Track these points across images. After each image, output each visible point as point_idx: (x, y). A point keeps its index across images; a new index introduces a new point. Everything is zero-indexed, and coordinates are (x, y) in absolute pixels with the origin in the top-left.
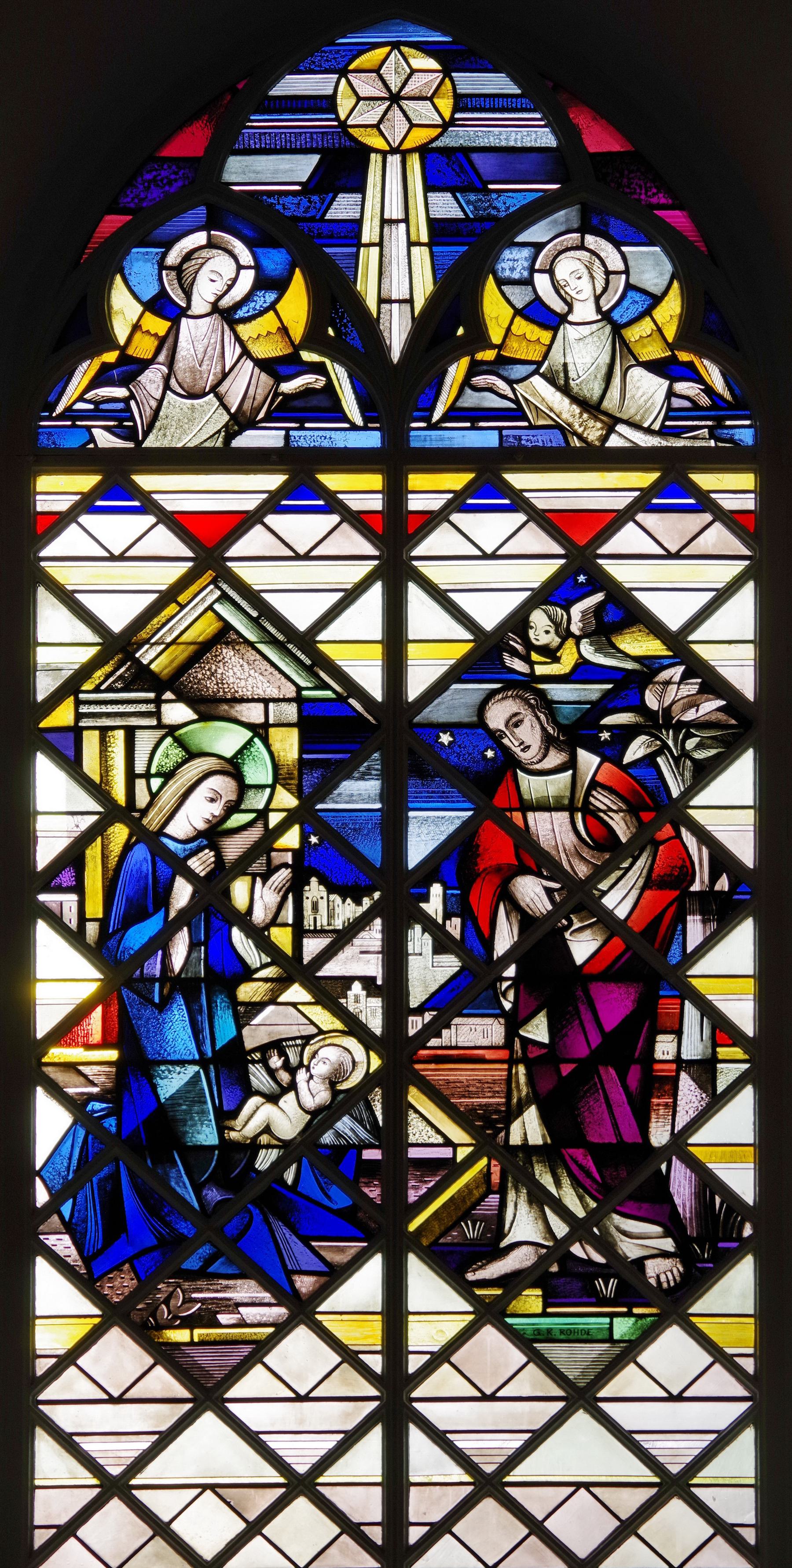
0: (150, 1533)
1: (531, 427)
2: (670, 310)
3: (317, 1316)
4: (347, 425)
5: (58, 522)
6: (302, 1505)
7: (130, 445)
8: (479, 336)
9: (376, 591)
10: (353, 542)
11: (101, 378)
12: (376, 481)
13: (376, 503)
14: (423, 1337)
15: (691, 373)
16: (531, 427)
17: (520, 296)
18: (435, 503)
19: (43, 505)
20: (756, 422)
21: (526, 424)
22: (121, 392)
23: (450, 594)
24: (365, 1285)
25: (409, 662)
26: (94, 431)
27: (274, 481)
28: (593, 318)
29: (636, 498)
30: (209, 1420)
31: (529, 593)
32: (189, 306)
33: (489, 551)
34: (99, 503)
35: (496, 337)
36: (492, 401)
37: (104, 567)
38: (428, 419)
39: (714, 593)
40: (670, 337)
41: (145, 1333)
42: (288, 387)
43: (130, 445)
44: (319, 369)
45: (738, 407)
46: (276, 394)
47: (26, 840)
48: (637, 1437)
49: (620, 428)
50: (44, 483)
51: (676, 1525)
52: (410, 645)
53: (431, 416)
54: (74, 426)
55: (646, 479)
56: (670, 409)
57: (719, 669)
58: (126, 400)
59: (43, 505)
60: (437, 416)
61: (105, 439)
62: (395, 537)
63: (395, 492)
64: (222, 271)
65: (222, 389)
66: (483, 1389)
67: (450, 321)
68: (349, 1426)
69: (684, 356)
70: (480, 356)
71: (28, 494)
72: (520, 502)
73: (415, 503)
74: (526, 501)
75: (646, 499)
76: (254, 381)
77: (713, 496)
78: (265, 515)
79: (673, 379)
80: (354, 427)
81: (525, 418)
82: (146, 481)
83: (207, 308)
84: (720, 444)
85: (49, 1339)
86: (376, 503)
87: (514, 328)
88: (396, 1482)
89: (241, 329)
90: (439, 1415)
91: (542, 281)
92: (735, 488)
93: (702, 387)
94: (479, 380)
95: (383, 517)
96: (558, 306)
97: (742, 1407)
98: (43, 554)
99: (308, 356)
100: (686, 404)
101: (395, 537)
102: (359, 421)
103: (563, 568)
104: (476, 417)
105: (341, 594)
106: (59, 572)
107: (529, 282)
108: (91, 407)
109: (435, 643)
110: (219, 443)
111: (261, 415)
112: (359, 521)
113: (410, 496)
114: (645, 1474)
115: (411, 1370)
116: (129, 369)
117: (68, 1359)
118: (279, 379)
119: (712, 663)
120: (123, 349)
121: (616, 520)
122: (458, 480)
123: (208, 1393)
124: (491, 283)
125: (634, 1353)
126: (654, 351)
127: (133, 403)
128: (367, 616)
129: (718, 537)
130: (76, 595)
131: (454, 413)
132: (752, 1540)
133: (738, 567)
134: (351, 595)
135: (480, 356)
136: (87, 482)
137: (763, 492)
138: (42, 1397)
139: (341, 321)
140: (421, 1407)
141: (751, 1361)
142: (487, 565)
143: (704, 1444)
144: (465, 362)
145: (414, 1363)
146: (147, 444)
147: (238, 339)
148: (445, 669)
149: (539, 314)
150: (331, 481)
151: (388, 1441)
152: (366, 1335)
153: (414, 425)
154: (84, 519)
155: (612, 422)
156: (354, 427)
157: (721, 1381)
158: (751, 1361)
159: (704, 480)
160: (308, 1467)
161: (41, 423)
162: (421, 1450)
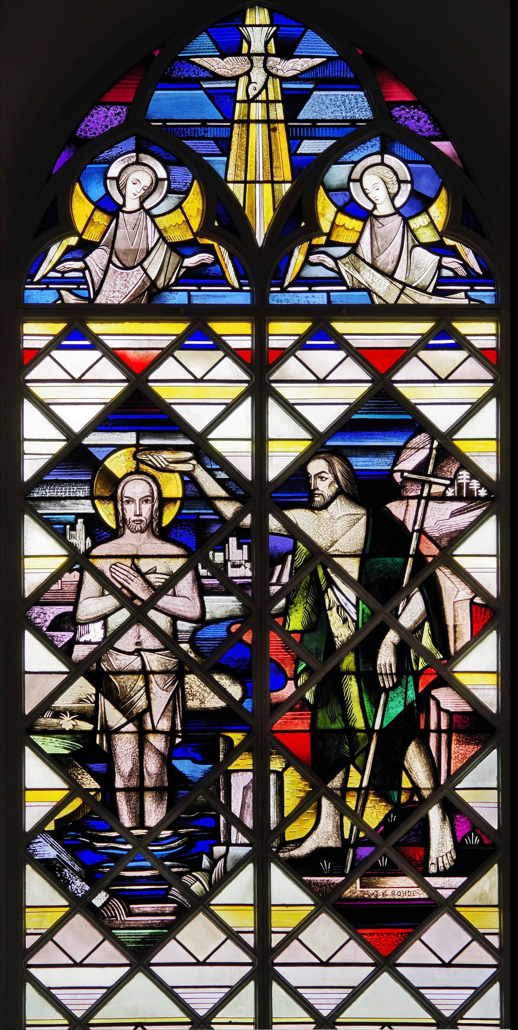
1: (349, 290)
3: (211, 907)
5: (38, 355)
9: (247, 404)
10: (229, 369)
12: (246, 327)
13: (246, 343)
14: (281, 921)
15: (454, 253)
18: (286, 343)
19: (28, 343)
22: (79, 265)
23: (296, 407)
24: (241, 887)
26: (62, 292)
28: (390, 229)
29: (50, 341)
32: (124, 205)
34: (65, 343)
35: (326, 227)
37: (69, 390)
38: (281, 285)
39: (470, 406)
41: (96, 917)
42: (190, 262)
44: (210, 249)
45: (485, 278)
47: (16, 456)
48: (422, 991)
49: (408, 290)
50: (28, 328)
53: (284, 283)
54: (48, 288)
55: (425, 327)
56: (440, 277)
58: (82, 270)
60: (286, 284)
61: (70, 299)
62: (260, 367)
63: (260, 335)
65: (145, 264)
67: (296, 218)
68: (233, 982)
69: (449, 242)
70: (315, 241)
71: (18, 336)
74: (346, 342)
75: (425, 341)
76: (167, 259)
77: (468, 338)
79: (441, 256)
80: (234, 290)
81: (344, 283)
82: (95, 327)
84: (472, 302)
85: (36, 923)
86: (246, 343)
87: (337, 222)
90: (292, 976)
93: (462, 263)
96: (368, 206)
97: (247, 969)
100: (451, 274)
101: (260, 367)
102: (237, 285)
104: (312, 283)
106: (39, 391)
107: (348, 189)
108: (60, 275)
111: (173, 280)
112: (236, 355)
113: (270, 338)
115: (273, 945)
116: (86, 248)
117: (47, 937)
118: (183, 257)
122: (302, 327)
123: (140, 957)
124: (321, 190)
126: (428, 236)
127: (87, 272)
128: (241, 420)
129: (474, 368)
131: (299, 280)
134: (231, 407)
135: (315, 241)
137: (500, 336)
139: (224, 217)
144: (305, 246)
145: (276, 939)
146: (98, 301)
147: (156, 226)
148: (292, 459)
149: (351, 209)
150: (218, 327)
152: (244, 921)
153: (272, 289)
154: (54, 353)
157: (477, 954)
159: (463, 328)
160: (206, 1011)
161: (26, 286)
162: (276, 415)
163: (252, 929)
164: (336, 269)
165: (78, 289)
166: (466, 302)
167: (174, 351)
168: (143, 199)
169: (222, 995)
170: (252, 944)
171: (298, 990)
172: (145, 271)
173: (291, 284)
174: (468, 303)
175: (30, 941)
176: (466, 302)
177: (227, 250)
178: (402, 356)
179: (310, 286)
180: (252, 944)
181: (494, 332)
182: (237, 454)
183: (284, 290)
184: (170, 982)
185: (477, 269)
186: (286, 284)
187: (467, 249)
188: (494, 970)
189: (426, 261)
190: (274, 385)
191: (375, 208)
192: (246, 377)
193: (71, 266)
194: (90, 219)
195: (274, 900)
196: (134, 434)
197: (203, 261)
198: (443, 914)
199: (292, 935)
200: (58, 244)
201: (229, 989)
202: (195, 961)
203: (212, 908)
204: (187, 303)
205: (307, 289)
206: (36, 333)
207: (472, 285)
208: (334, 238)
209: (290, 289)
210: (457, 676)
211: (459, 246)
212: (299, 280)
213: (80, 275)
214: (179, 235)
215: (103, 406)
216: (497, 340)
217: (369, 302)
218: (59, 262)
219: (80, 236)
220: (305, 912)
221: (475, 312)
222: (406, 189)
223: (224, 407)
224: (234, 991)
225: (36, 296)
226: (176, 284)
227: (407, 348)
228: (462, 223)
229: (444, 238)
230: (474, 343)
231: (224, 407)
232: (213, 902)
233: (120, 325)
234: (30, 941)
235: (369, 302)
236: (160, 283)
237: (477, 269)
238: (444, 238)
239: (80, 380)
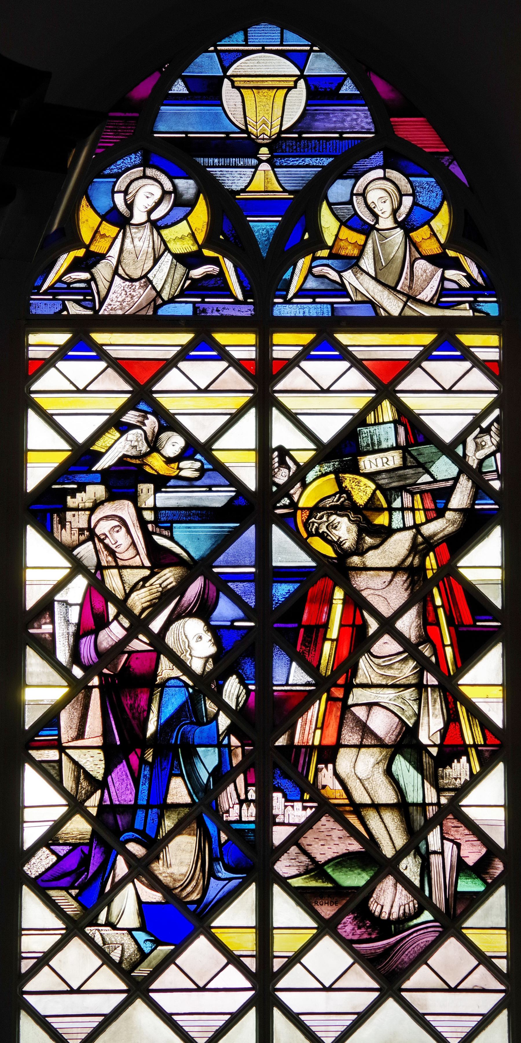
1: (352, 302)
4: (232, 300)
5: (45, 365)
7: (89, 312)
8: (318, 241)
10: (234, 379)
11: (75, 266)
12: (251, 338)
13: (250, 354)
14: (284, 945)
15: (457, 265)
16: (352, 302)
18: (290, 353)
19: (33, 353)
20: (499, 299)
21: (348, 300)
22: (85, 276)
23: (55, 417)
25: (28, 465)
27: (185, 338)
29: (421, 351)
30: (139, 1007)
31: (107, 417)
33: (325, 387)
37: (72, 402)
42: (197, 273)
43: (89, 312)
44: (215, 261)
46: (187, 278)
50: (33, 338)
55: (428, 338)
58: (87, 282)
59: (33, 353)
60: (290, 296)
61: (74, 309)
62: (264, 377)
63: (264, 346)
64: (146, 193)
68: (485, 1010)
69: (451, 253)
71: (24, 346)
72: (346, 353)
73: (278, 353)
74: (350, 353)
77: (472, 350)
81: (348, 296)
83: (144, 218)
84: (476, 314)
86: (250, 354)
87: (340, 236)
89: (164, 232)
92: (487, 345)
93: (465, 274)
96: (368, 218)
97: (249, 995)
99: (207, 253)
100: (455, 286)
101: (264, 377)
102: (240, 297)
105: (229, 417)
107: (351, 202)
108: (65, 286)
110: (150, 313)
112: (239, 365)
115: (276, 969)
116: (90, 261)
121: (166, 365)
124: (325, 204)
126: (431, 248)
127: (92, 283)
128: (245, 432)
129: (478, 380)
134: (235, 418)
136: (62, 338)
137: (505, 348)
141: (505, 961)
142: (324, 396)
144: (309, 258)
145: (277, 964)
148: (50, 470)
149: (353, 223)
150: (222, 338)
152: (245, 944)
153: (276, 300)
154: (304, 364)
156: (237, 302)
157: (482, 977)
158: (505, 961)
159: (466, 339)
161: (32, 297)
163: (505, 954)
165: (85, 300)
166: (470, 313)
167: (421, 362)
168: (150, 212)
169: (474, 1024)
170: (253, 969)
171: (425, 1017)
174: (472, 315)
175: (25, 966)
176: (470, 313)
178: (406, 367)
179: (314, 297)
180: (253, 969)
181: (497, 344)
183: (288, 302)
184: (168, 1009)
185: (480, 280)
186: (290, 296)
188: (502, 995)
190: (276, 395)
191: (377, 222)
192: (251, 387)
193: (78, 277)
195: (276, 923)
198: (197, 937)
199: (294, 959)
201: (481, 1017)
203: (213, 930)
207: (475, 297)
209: (295, 300)
210: (462, 689)
211: (461, 258)
214: (188, 247)
215: (351, 417)
219: (87, 247)
220: (308, 935)
221: (479, 324)
222: (408, 201)
223: (229, 417)
225: (42, 306)
227: (409, 360)
228: (465, 235)
229: (447, 250)
232: (465, 925)
234: (25, 966)
235: (373, 314)
236: (165, 295)
237: (480, 280)
238: (447, 250)
239: (206, 390)
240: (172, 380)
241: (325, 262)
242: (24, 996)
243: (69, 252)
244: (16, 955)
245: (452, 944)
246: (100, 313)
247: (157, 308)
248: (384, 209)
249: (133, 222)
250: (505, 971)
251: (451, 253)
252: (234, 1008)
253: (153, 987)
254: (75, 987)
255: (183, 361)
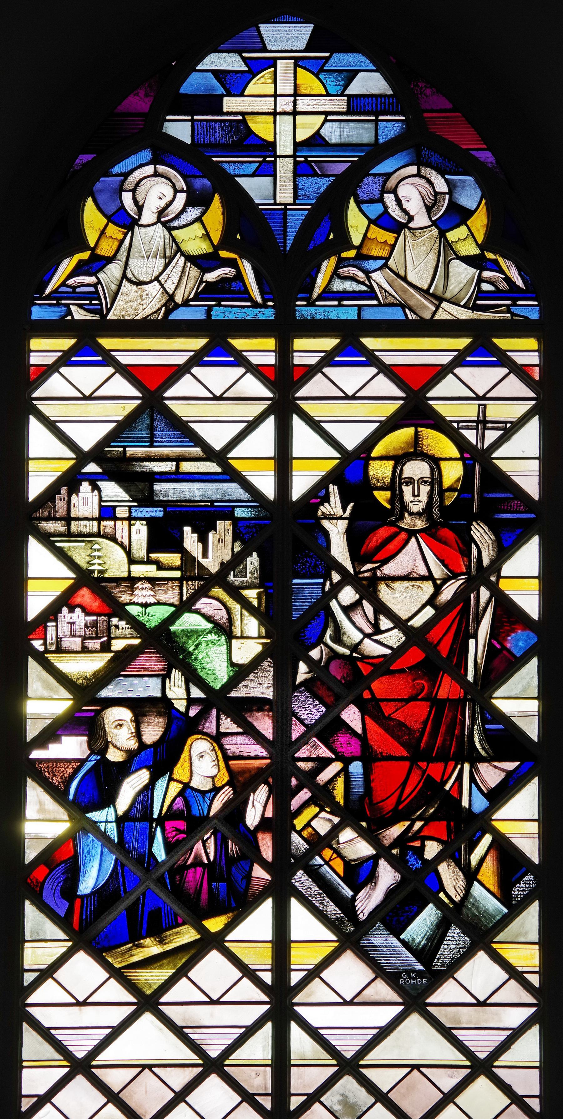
0: (105, 1100)
1: (380, 305)
2: (479, 222)
4: (249, 304)
5: (46, 372)
6: (214, 1080)
8: (344, 240)
9: (270, 423)
10: (253, 386)
11: (79, 270)
12: (270, 343)
13: (270, 359)
14: (302, 959)
17: (375, 210)
18: (312, 360)
19: (35, 359)
21: (375, 302)
22: (92, 280)
27: (198, 343)
28: (423, 242)
30: (148, 1019)
31: (115, 424)
35: (356, 240)
36: (349, 286)
40: (480, 239)
42: (211, 277)
46: (202, 281)
49: (444, 305)
50: (35, 343)
51: (483, 1094)
52: (294, 461)
57: (513, 478)
58: (95, 285)
59: (35, 359)
60: (315, 295)
61: (79, 314)
62: (285, 383)
63: (284, 352)
64: (156, 190)
66: (344, 1003)
69: (490, 256)
70: (344, 255)
73: (298, 359)
74: (377, 358)
77: (245, 354)
78: (192, 367)
79: (482, 269)
80: (255, 305)
81: (376, 298)
83: (154, 218)
86: (270, 359)
88: (281, 1063)
89: (174, 233)
90: (313, 1016)
91: (389, 199)
92: (525, 350)
93: (503, 276)
94: (343, 271)
95: (275, 369)
96: (401, 218)
97: (530, 1011)
98: (35, 395)
99: (224, 254)
100: (491, 288)
101: (285, 383)
102: (259, 300)
103: (402, 407)
105: (246, 424)
107: (381, 200)
108: (71, 290)
109: (312, 457)
111: (192, 296)
112: (258, 371)
114: (460, 1058)
116: (96, 263)
119: (508, 473)
120: (93, 249)
122: (329, 343)
125: (452, 971)
126: (470, 249)
127: (99, 286)
128: (263, 440)
129: (514, 386)
130: (57, 424)
131: (327, 294)
132: (537, 1109)
133: (529, 405)
134: (252, 426)
135: (344, 255)
138: (29, 1001)
140: (300, 1010)
142: (349, 404)
143: (503, 1038)
144: (333, 260)
145: (295, 978)
149: (385, 221)
151: (276, 1042)
152: (261, 959)
153: (298, 303)
155: (439, 299)
156: (255, 305)
157: (513, 992)
160: (85, 1053)
162: (301, 432)
164: (367, 282)
172: (162, 286)
173: (320, 298)
177: (514, 263)
181: (536, 347)
182: (525, 473)
183: (311, 304)
185: (520, 283)
186: (315, 295)
187: (509, 263)
188: (534, 1009)
189: (462, 274)
194: (103, 233)
195: (294, 936)
196: (128, 454)
197: (225, 276)
199: (314, 973)
200: (68, 259)
202: (208, 1000)
204: (356, 318)
205: (336, 303)
206: (43, 350)
207: (514, 300)
208: (365, 251)
209: (318, 303)
211: (501, 260)
212: (327, 294)
213: (92, 289)
216: (540, 356)
217: (404, 318)
218: (71, 276)
221: (518, 328)
224: (250, 1031)
226: (196, 298)
230: (515, 359)
231: (244, 425)
233: (380, 340)
234: (29, 978)
235: (404, 318)
236: (179, 299)
237: (520, 283)
240: (184, 386)
241: (352, 263)
242: (27, 1008)
243: (73, 256)
244: (17, 967)
245: (481, 957)
246: (108, 318)
247: (168, 312)
248: (415, 205)
249: (140, 223)
250: (537, 985)
251: (490, 256)
252: (249, 1021)
253: (163, 1000)
254: (81, 999)
255: (196, 366)
